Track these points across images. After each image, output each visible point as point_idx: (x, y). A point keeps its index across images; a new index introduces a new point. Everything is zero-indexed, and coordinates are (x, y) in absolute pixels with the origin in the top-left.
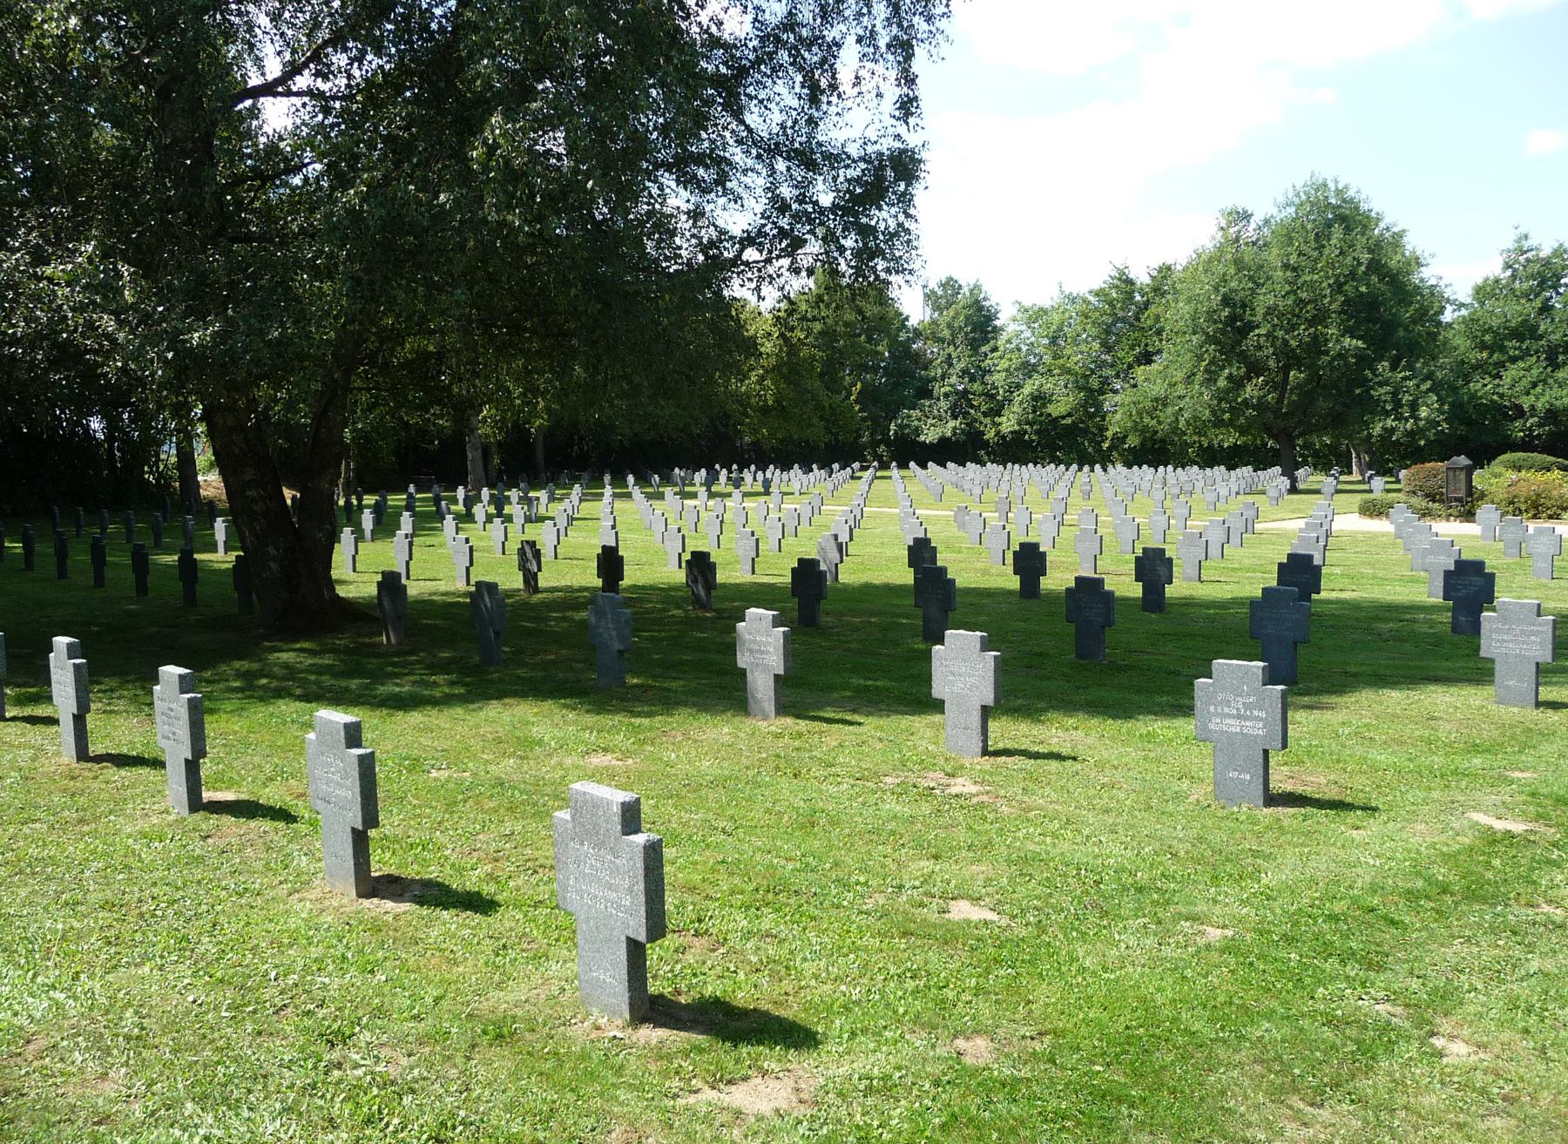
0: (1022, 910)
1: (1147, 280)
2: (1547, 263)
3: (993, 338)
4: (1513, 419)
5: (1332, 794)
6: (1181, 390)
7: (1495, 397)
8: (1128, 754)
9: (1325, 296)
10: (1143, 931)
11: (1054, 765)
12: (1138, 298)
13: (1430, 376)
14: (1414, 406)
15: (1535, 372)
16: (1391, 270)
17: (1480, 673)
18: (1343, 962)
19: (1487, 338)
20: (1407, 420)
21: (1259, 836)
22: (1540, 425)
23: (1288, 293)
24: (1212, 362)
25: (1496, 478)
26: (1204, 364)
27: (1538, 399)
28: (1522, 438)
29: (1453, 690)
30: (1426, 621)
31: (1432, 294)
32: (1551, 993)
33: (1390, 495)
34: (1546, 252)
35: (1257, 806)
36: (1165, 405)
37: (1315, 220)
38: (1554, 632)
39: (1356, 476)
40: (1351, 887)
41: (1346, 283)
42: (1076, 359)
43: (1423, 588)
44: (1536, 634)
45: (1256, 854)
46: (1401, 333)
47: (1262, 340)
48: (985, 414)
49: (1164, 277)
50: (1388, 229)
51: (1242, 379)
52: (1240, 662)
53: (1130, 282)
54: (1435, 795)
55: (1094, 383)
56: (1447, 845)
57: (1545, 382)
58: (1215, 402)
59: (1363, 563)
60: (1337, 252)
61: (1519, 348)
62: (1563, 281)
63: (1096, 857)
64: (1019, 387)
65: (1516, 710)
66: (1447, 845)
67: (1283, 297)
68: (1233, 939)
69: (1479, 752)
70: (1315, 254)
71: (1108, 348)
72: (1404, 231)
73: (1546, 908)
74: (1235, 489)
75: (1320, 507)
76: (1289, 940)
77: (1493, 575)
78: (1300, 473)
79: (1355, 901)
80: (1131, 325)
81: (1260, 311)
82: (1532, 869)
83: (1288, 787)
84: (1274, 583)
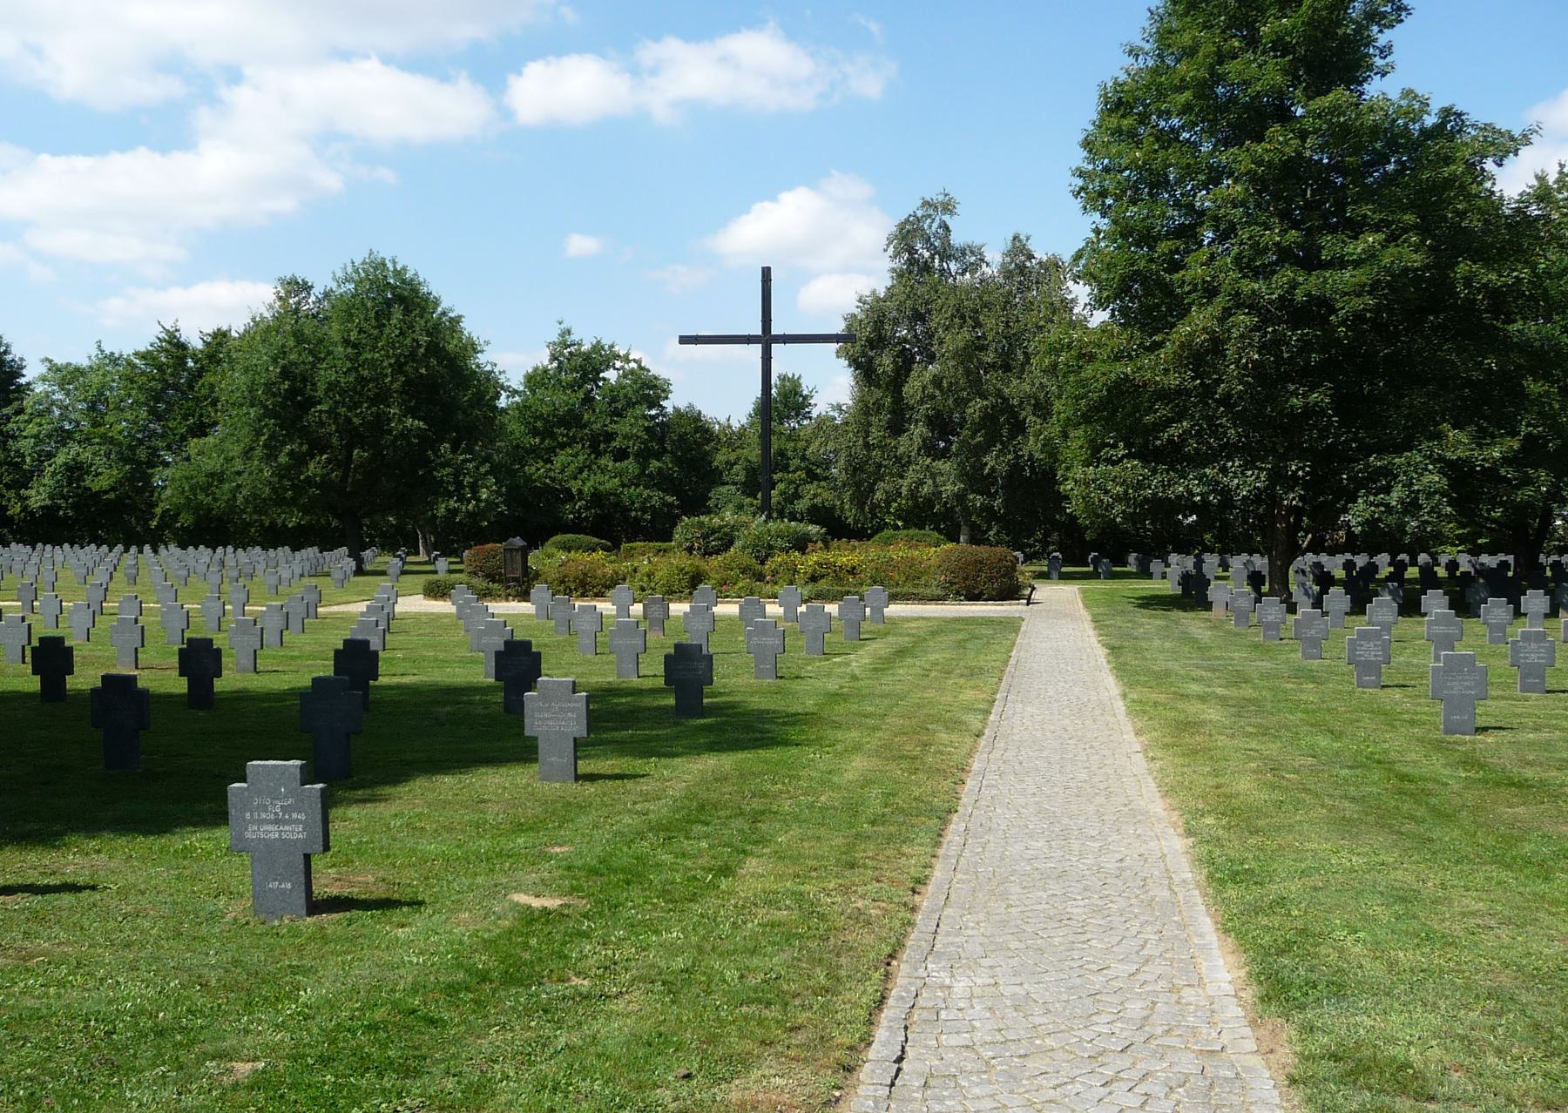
0: (10, 1084)
1: (199, 345)
2: (587, 357)
3: (17, 399)
4: (564, 502)
5: (380, 892)
6: (238, 465)
7: (547, 481)
8: (158, 874)
9: (386, 375)
10: (161, 1081)
11: (67, 899)
12: (191, 364)
13: (487, 459)
14: (474, 488)
15: (581, 458)
16: (448, 353)
17: (525, 752)
18: (380, 1075)
19: (539, 424)
20: (469, 502)
21: (300, 949)
22: (587, 508)
23: (349, 370)
24: (271, 437)
25: (549, 558)
26: (263, 438)
27: (584, 483)
28: (572, 520)
29: (503, 770)
30: (482, 702)
31: (488, 380)
32: (575, 1067)
33: (453, 576)
34: (586, 347)
35: (299, 917)
36: (221, 481)
37: (374, 299)
38: (588, 707)
39: (423, 557)
40: (393, 991)
41: (406, 363)
42: (120, 427)
43: (480, 669)
44: (572, 710)
45: (295, 970)
46: (460, 417)
47: (324, 416)
48: (8, 487)
49: (220, 344)
50: (444, 313)
51: (305, 454)
52: (259, 762)
53: (182, 346)
54: (479, 880)
55: (142, 454)
56: (490, 931)
57: (589, 468)
58: (276, 479)
59: (425, 645)
60: (397, 332)
61: (567, 435)
62: (601, 375)
63: (110, 1002)
64: (50, 455)
65: (558, 785)
66: (490, 931)
67: (345, 373)
68: (264, 1071)
69: (523, 831)
70: (376, 332)
71: (156, 415)
72: (460, 317)
73: (575, 981)
74: (298, 571)
75: (384, 590)
76: (325, 1061)
77: (539, 654)
78: (367, 554)
79: (395, 1004)
80: (184, 393)
81: (322, 386)
82: (564, 944)
83: (334, 891)
84: (330, 672)
